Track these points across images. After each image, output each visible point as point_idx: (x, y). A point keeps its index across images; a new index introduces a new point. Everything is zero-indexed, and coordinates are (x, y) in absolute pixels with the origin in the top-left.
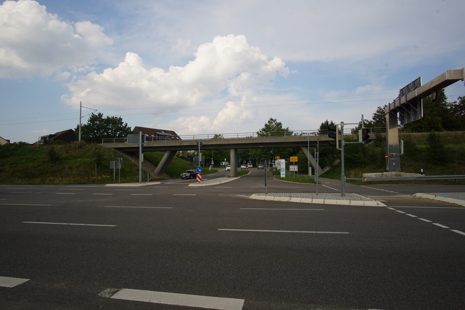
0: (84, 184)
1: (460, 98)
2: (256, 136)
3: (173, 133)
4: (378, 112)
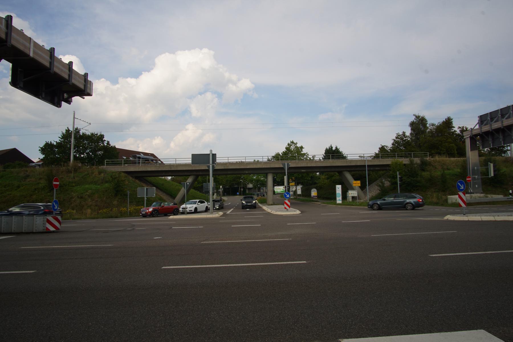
0: (116, 217)
1: (459, 127)
4: (397, 138)
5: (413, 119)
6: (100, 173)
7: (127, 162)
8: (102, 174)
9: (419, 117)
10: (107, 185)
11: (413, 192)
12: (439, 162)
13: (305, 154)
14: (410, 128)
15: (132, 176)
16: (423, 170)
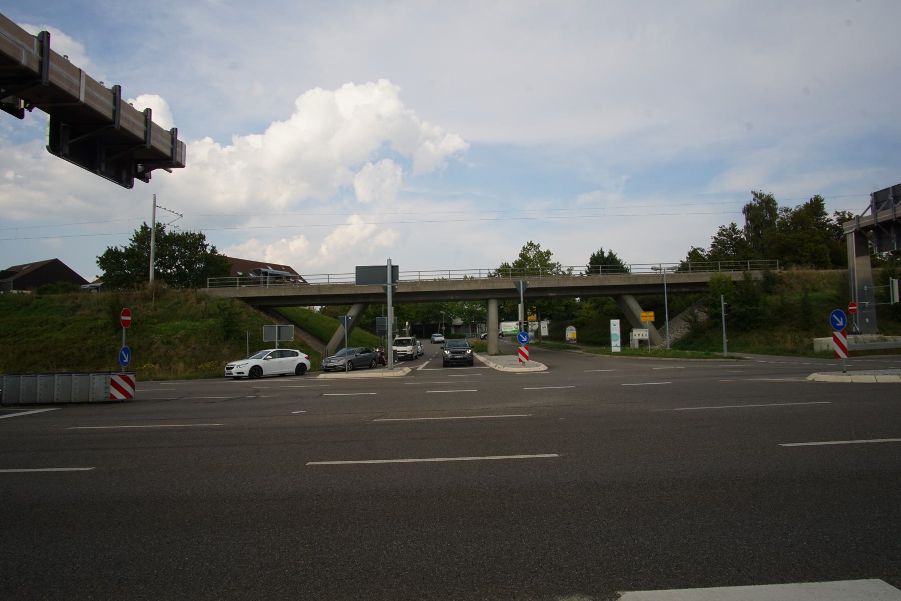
1: (837, 213)
2: (352, 279)
3: (288, 269)
4: (720, 234)
5: (749, 199)
6: (199, 300)
8: (203, 303)
9: (761, 195)
10: (211, 321)
12: (798, 277)
13: (554, 265)
14: (744, 217)
16: (769, 292)
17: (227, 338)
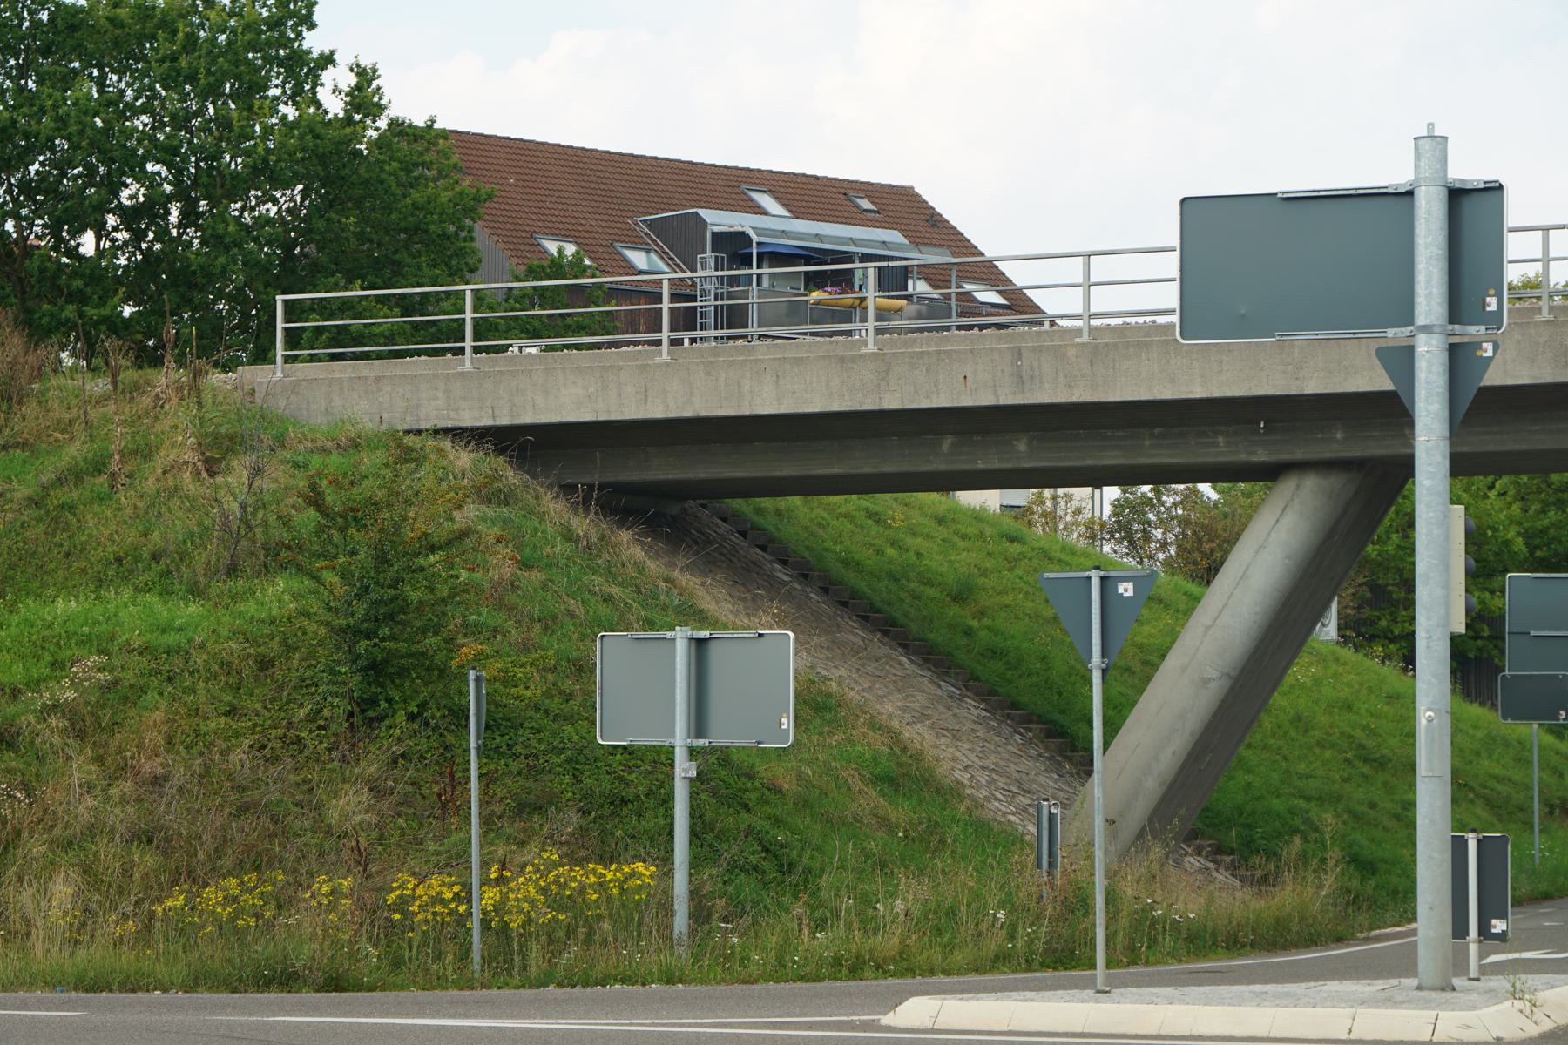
0: (335, 983)
2: (1152, 289)
3: (901, 206)
6: (216, 452)
7: (573, 313)
8: (237, 475)
10: (278, 594)
11: (907, 655)
15: (568, 489)
17: (366, 713)
